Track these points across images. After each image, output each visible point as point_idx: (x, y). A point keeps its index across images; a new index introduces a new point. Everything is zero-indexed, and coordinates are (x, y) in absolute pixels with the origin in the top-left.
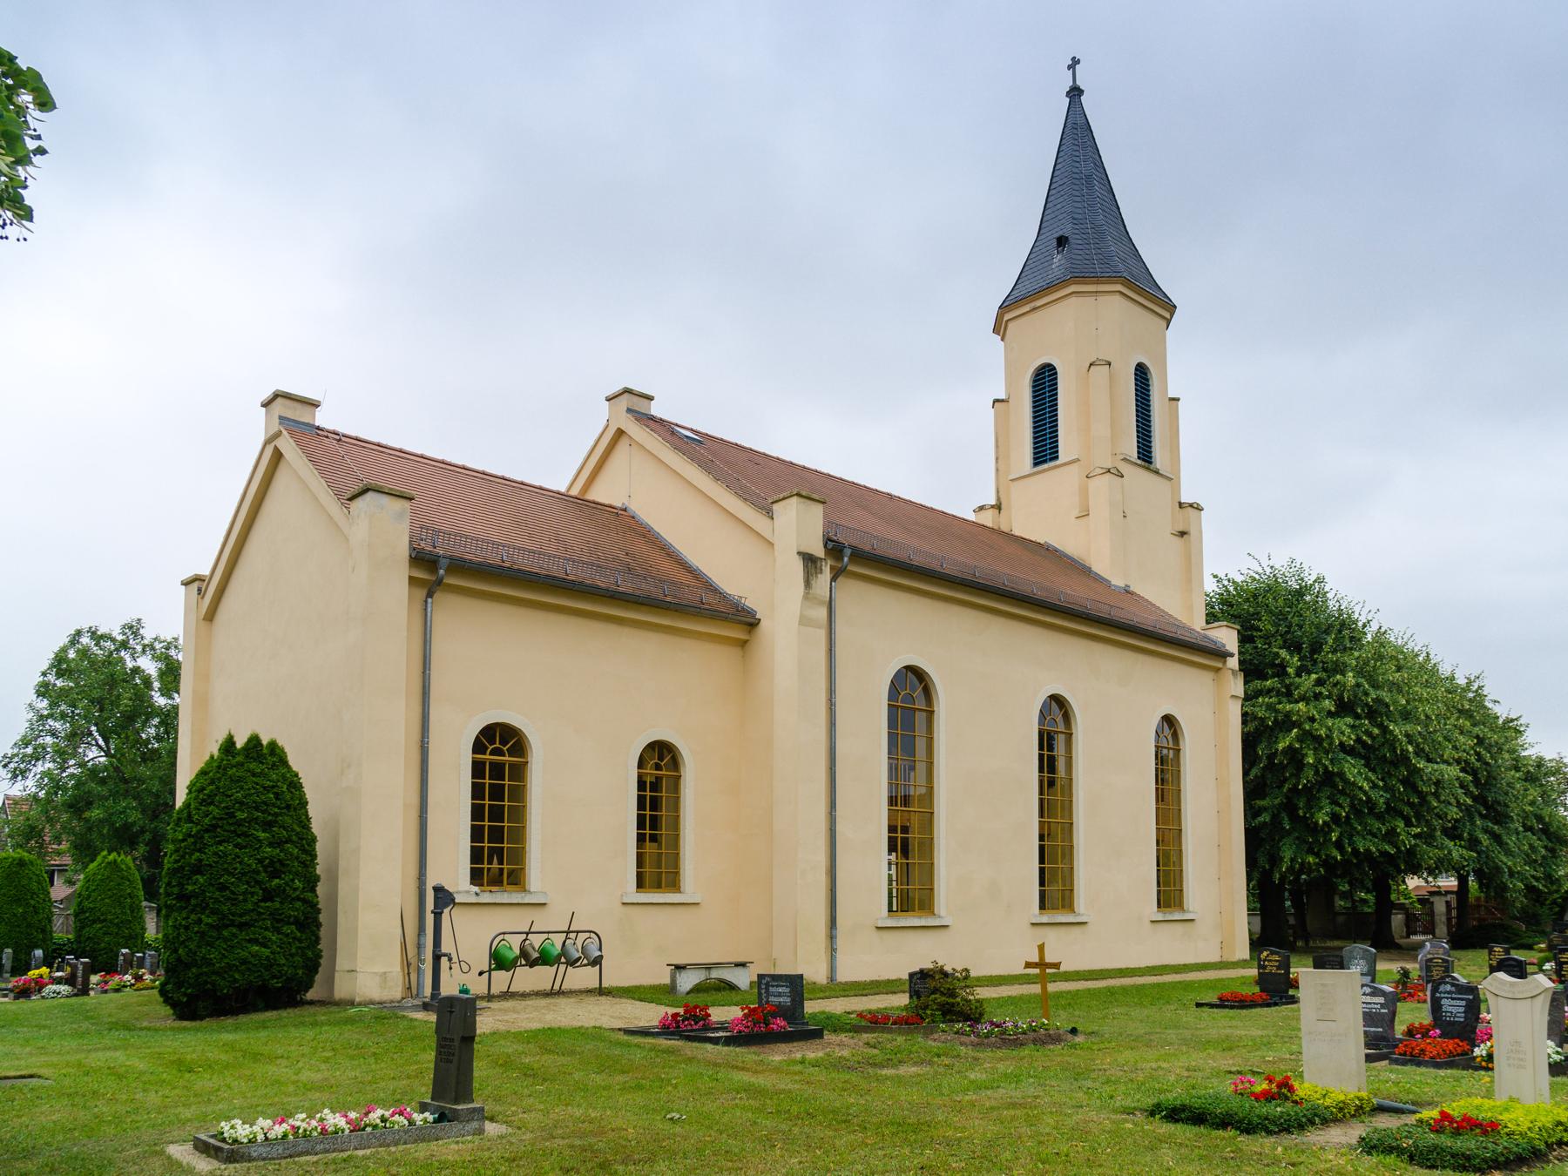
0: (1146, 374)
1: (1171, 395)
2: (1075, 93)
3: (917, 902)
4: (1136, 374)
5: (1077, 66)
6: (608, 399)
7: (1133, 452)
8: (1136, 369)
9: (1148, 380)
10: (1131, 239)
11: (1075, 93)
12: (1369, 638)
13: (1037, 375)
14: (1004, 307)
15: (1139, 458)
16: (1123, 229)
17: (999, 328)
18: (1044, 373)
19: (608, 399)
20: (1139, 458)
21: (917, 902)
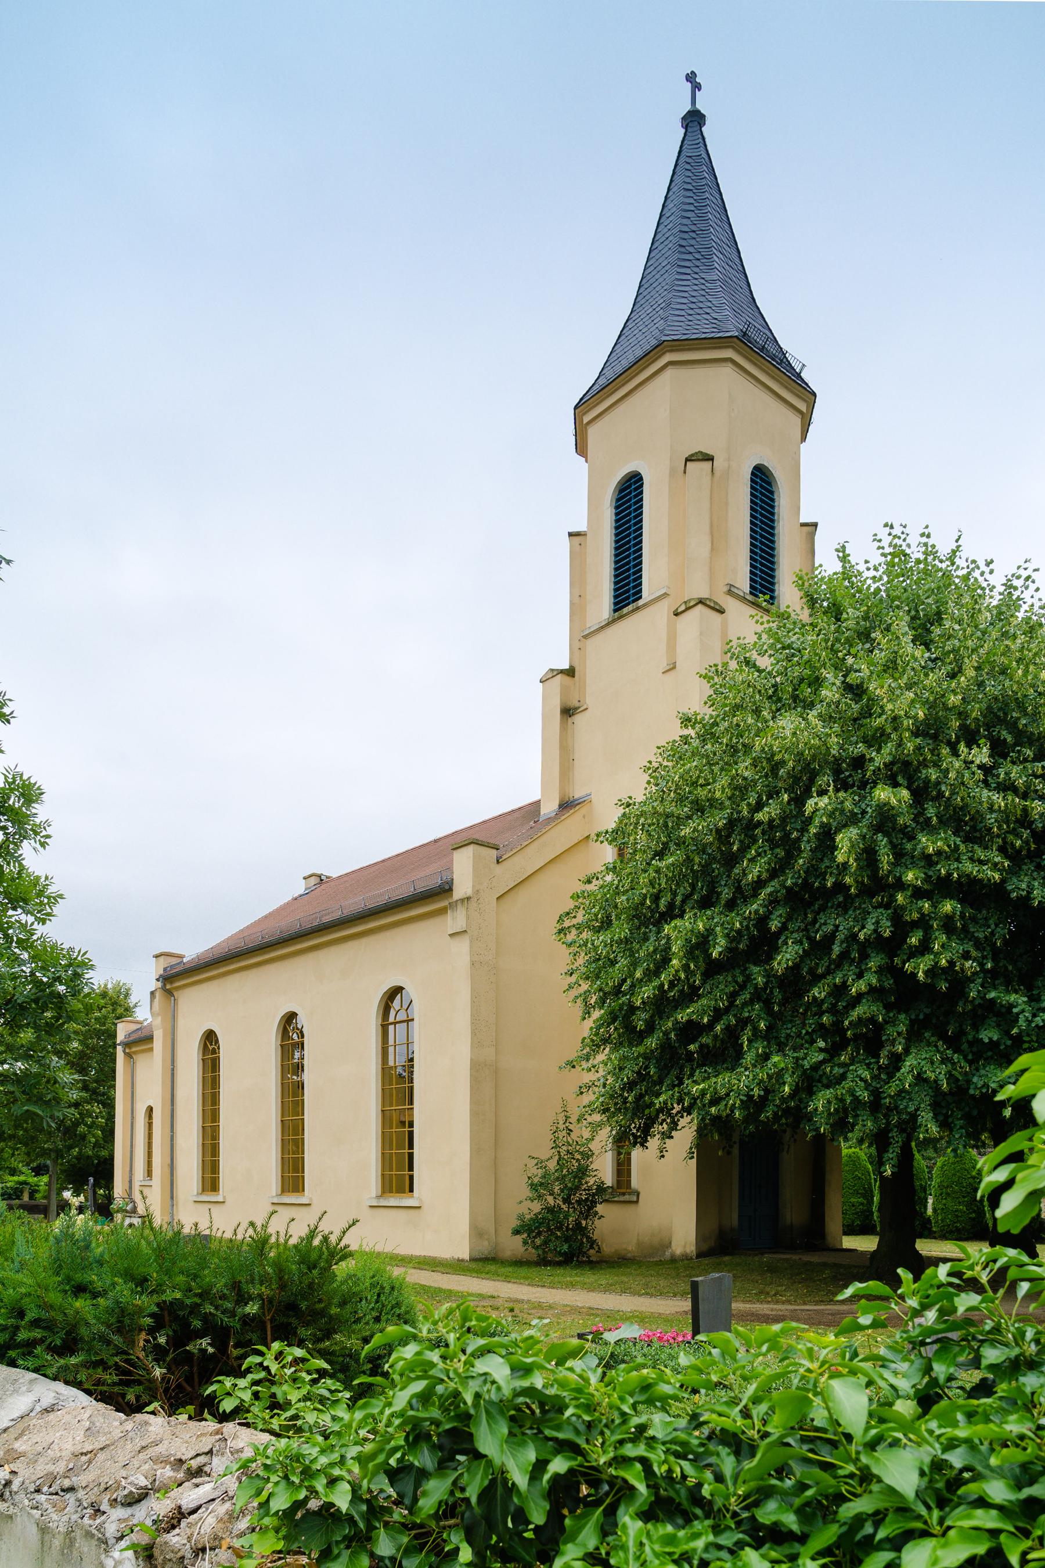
0: (769, 484)
1: (803, 519)
2: (694, 120)
3: (269, 1333)
4: (752, 480)
5: (1015, 1231)
6: (305, 878)
7: (744, 584)
8: (753, 474)
9: (772, 493)
10: (713, 170)
11: (694, 120)
12: (1020, 615)
13: (621, 491)
14: (581, 406)
15: (751, 593)
16: (745, 286)
17: (581, 448)
18: (630, 486)
19: (305, 878)
20: (751, 593)
21: (269, 1333)
